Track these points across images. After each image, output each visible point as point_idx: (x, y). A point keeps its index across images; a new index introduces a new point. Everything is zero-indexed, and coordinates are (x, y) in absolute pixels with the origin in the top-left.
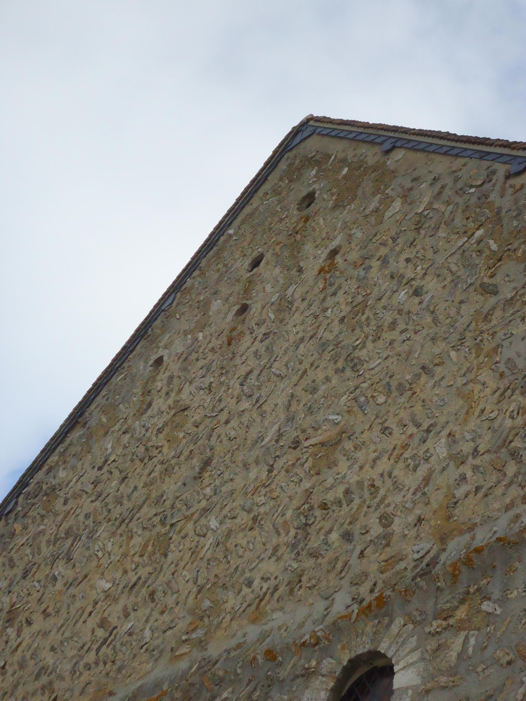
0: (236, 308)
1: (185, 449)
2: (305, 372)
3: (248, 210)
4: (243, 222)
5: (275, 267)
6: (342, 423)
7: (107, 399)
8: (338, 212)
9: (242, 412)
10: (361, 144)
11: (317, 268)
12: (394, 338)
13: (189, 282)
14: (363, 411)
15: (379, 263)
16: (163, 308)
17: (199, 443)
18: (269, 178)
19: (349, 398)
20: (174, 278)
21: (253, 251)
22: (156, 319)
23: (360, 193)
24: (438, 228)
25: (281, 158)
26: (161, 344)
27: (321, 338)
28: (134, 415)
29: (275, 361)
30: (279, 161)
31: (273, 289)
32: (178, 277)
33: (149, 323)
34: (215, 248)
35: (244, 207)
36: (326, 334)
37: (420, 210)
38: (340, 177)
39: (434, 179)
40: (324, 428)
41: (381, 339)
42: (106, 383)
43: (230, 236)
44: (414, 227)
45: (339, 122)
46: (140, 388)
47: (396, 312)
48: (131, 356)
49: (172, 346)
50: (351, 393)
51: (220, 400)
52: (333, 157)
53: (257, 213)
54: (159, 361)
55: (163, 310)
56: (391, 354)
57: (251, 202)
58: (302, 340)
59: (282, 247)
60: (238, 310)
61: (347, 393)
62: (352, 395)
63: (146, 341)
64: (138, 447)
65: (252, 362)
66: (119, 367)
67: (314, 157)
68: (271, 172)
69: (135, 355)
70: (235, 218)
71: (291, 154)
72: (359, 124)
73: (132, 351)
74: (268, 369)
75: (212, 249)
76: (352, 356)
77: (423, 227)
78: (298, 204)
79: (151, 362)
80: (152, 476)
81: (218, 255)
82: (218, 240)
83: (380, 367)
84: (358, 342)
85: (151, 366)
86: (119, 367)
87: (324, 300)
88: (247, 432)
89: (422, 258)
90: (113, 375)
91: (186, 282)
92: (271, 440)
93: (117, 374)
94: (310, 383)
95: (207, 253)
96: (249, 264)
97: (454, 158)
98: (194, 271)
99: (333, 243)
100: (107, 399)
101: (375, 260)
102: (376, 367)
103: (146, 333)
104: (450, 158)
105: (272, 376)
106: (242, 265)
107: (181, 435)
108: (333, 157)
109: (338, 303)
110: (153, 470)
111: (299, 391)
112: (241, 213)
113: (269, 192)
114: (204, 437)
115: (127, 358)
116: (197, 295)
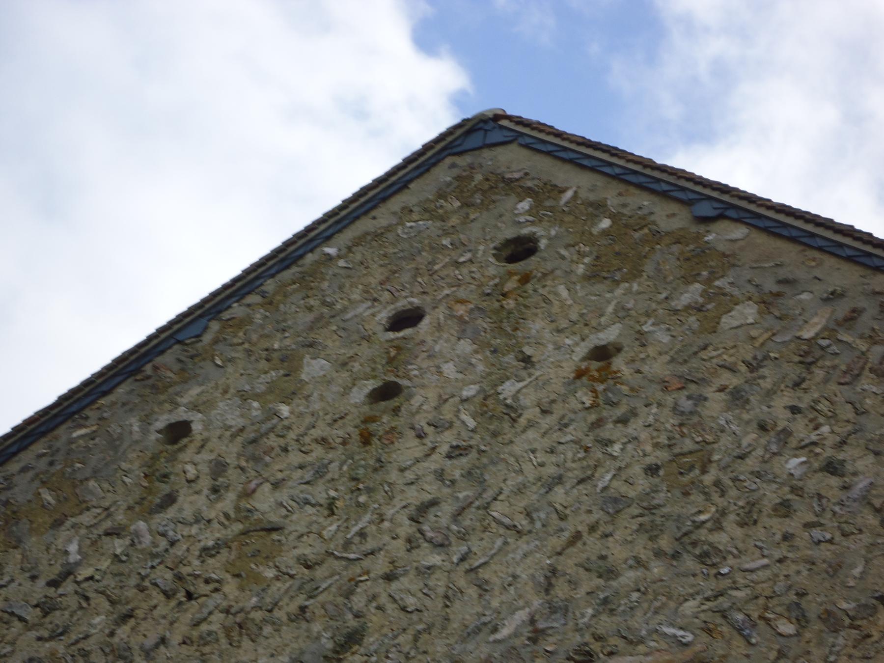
0: (371, 385)
1: (286, 600)
2: (577, 536)
3: (365, 225)
4: (358, 242)
5: (459, 339)
6: (698, 647)
7: (51, 464)
8: (599, 287)
9: (429, 568)
10: (632, 190)
11: (568, 370)
12: (791, 531)
13: (237, 310)
14: (747, 639)
15: (722, 396)
16: (180, 337)
17: (321, 598)
18: (412, 186)
19: (704, 607)
20: (204, 293)
21: (395, 299)
22: (162, 352)
23: (649, 268)
24: (858, 375)
25: (439, 161)
26: (184, 400)
27: (605, 489)
28: (130, 508)
29: (495, 499)
30: (434, 164)
31: (460, 376)
32: (214, 295)
33: (145, 355)
34: (294, 269)
35: (358, 218)
36: (615, 484)
37: (807, 334)
38: (595, 231)
39: (832, 293)
40: (652, 644)
41: (759, 525)
42: (43, 434)
43: (329, 258)
44: (797, 359)
45: (581, 140)
46: (137, 464)
47: (787, 489)
48: (102, 401)
49: (217, 407)
50: (708, 599)
51: (362, 534)
52: (569, 194)
53: (391, 236)
54: (178, 432)
55: (179, 342)
56: (790, 555)
57: (374, 213)
58: (559, 480)
59: (472, 310)
60: (375, 390)
61: (699, 598)
62: (710, 604)
63: (137, 384)
64: (153, 567)
65: (432, 489)
66: (74, 413)
67: (517, 180)
68: (418, 177)
69: (114, 403)
70: (340, 231)
71: (464, 161)
72: (630, 157)
73: (105, 394)
74: (478, 508)
75: (288, 267)
76: (694, 537)
77: (820, 363)
78: (495, 248)
79: (160, 424)
80: (204, 627)
81: (305, 281)
82: (301, 257)
83: (768, 573)
84: (703, 517)
85: (159, 432)
86: (74, 413)
87: (598, 424)
88: (447, 606)
89: (830, 414)
90: (62, 423)
91: (229, 307)
92: (516, 634)
93: (69, 424)
94: (594, 558)
95: (278, 272)
96: (389, 318)
97: (869, 272)
98: (249, 293)
99: (601, 335)
100: (51, 464)
101: (711, 390)
102: (758, 569)
103: (138, 370)
104: (857, 268)
105: (493, 524)
106: (374, 315)
107: (270, 573)
108: (569, 194)
109: (636, 438)
110: (205, 619)
111: (568, 564)
112: (353, 227)
113: (415, 209)
114: (333, 589)
115: (93, 402)
116: (261, 336)
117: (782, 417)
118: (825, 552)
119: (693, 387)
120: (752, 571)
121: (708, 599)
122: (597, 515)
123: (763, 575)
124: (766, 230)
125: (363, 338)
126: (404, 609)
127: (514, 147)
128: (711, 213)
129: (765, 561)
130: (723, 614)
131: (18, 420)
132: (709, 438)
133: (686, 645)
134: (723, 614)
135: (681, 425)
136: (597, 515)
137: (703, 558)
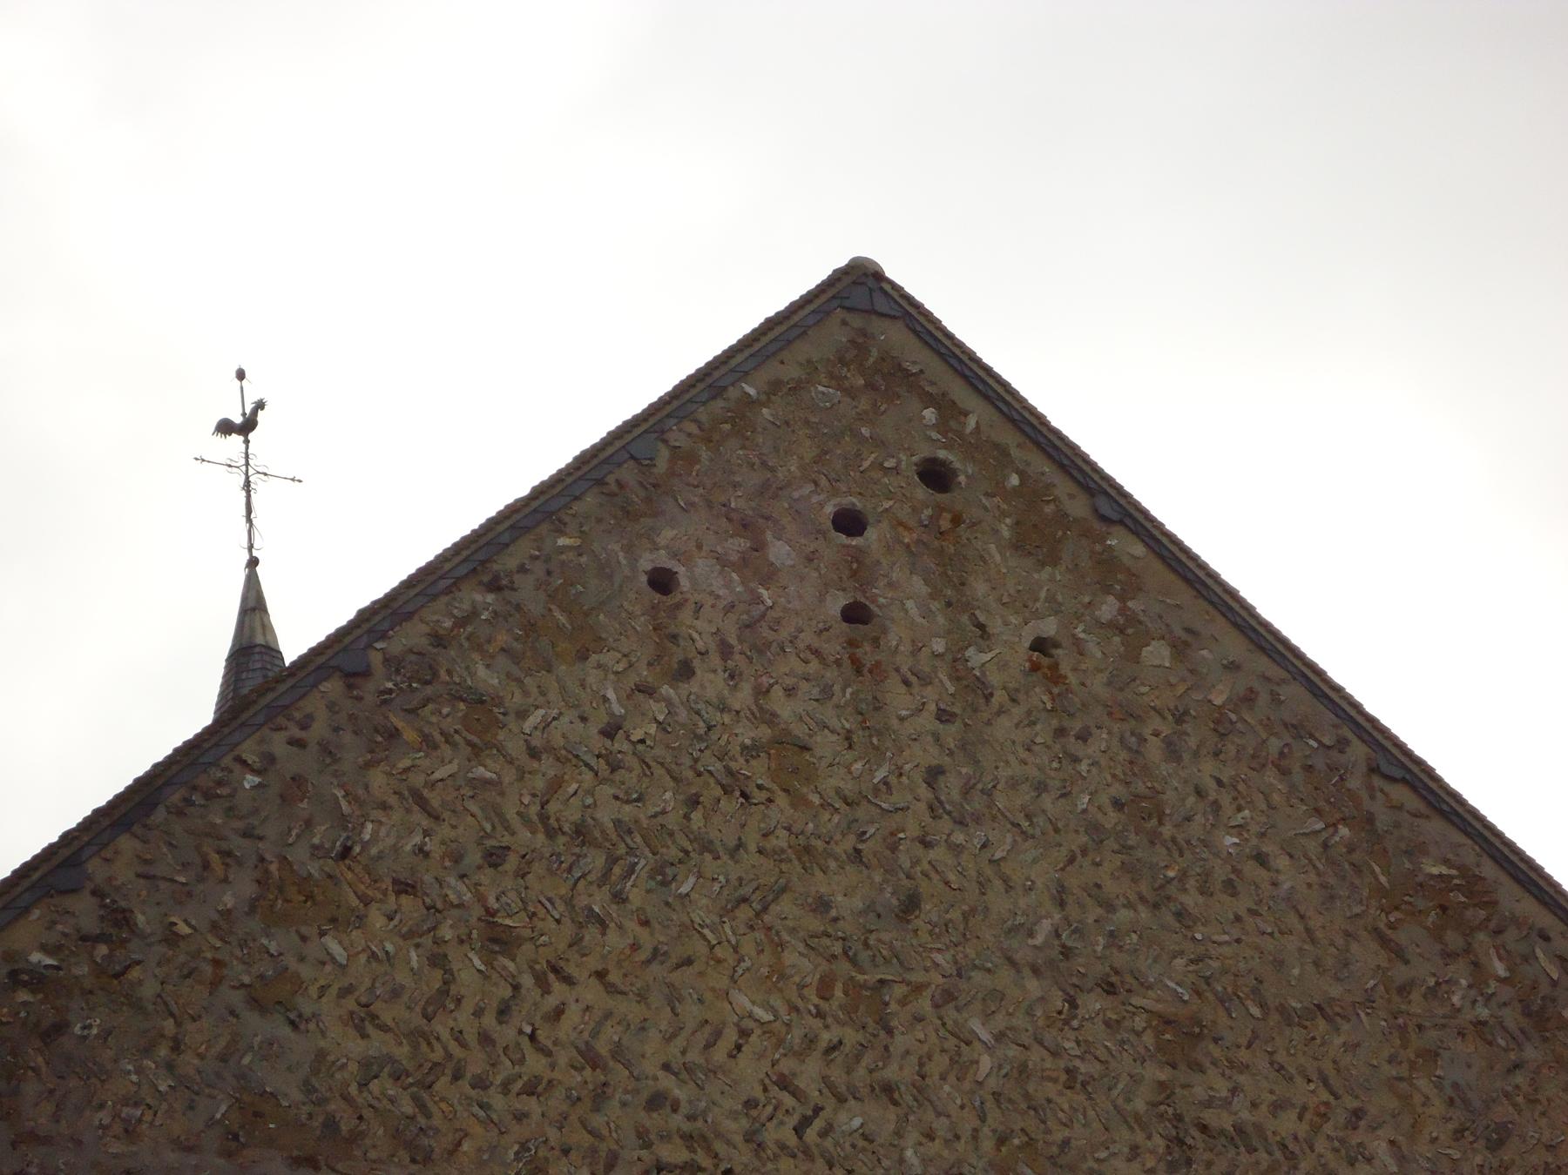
14: (1228, 1011)
50: (1192, 961)
117: (531, 1105)
118: (1269, 944)
119: (1133, 722)
120: (1220, 944)
121: (1192, 961)
122: (1084, 839)
123: (1226, 950)
124: (1162, 558)
125: (819, 532)
126: (947, 883)
127: (900, 324)
128: (1115, 517)
129: (1226, 938)
130: (1207, 980)
131: (1386, 721)
132: (1159, 788)
133: (1185, 1002)
134: (1207, 980)
135: (1131, 763)
136: (1084, 839)
137: (1180, 915)
